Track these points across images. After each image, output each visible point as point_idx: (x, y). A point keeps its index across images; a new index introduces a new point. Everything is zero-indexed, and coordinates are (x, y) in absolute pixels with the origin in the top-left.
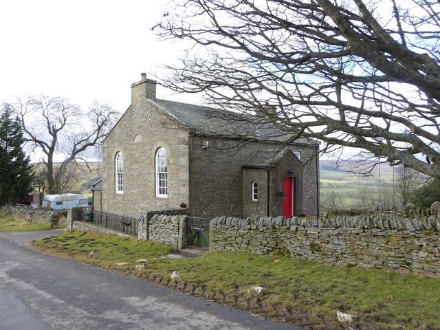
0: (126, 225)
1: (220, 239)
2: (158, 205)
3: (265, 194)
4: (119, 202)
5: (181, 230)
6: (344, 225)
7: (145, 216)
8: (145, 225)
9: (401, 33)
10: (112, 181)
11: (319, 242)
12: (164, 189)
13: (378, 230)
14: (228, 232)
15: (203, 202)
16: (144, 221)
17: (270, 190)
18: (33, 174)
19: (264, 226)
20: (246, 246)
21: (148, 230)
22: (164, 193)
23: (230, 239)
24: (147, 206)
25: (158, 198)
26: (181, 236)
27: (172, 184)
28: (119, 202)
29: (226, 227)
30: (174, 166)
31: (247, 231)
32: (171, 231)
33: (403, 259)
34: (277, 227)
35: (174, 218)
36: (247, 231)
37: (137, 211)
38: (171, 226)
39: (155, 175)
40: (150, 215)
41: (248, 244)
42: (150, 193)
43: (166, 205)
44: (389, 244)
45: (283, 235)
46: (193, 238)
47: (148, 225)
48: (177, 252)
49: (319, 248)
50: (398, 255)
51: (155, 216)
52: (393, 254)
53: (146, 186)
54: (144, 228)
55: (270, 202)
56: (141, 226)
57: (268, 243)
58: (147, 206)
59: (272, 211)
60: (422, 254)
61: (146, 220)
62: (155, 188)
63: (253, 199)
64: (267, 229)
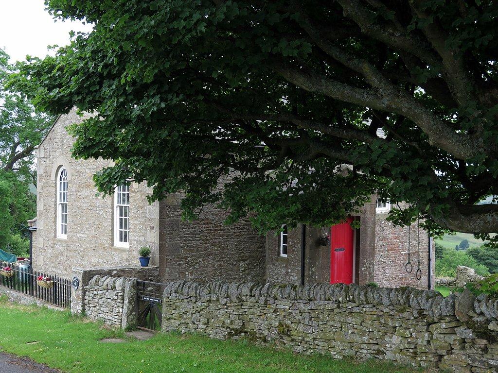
0: (56, 292)
1: (174, 316)
2: (117, 260)
3: (299, 246)
4: (62, 254)
5: (126, 302)
6: (318, 297)
7: (80, 277)
8: (80, 292)
9: (194, 100)
10: (51, 215)
11: (289, 322)
12: (125, 232)
13: (354, 305)
14: (184, 304)
15: (187, 257)
16: (78, 285)
17: (307, 238)
18: (89, 111)
19: (228, 297)
20: (204, 327)
21: (84, 299)
22: (125, 241)
23: (185, 316)
24: (101, 261)
25: (116, 249)
26: (125, 311)
27: (135, 225)
28: (62, 254)
29: (181, 297)
30: (139, 194)
31: (206, 304)
32: (113, 303)
33: (377, 346)
34: (244, 298)
35: (119, 282)
36: (206, 304)
37: (69, 271)
38: (111, 294)
39: (113, 208)
40: (88, 276)
41: (207, 324)
42: (105, 240)
43: (127, 260)
44: (363, 324)
45: (251, 311)
46: (144, 315)
47: (84, 292)
48: (120, 336)
49: (288, 330)
50: (371, 341)
51: (95, 277)
52: (366, 338)
53: (99, 226)
54: (78, 297)
55: (307, 261)
56: (75, 294)
57: (232, 322)
58: (101, 261)
59: (309, 276)
60: (396, 339)
61: (80, 284)
62: (112, 230)
63: (282, 255)
64: (231, 301)
